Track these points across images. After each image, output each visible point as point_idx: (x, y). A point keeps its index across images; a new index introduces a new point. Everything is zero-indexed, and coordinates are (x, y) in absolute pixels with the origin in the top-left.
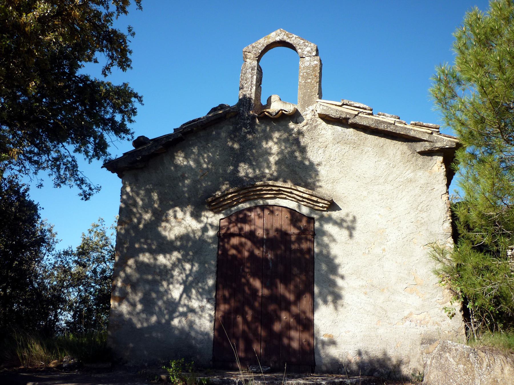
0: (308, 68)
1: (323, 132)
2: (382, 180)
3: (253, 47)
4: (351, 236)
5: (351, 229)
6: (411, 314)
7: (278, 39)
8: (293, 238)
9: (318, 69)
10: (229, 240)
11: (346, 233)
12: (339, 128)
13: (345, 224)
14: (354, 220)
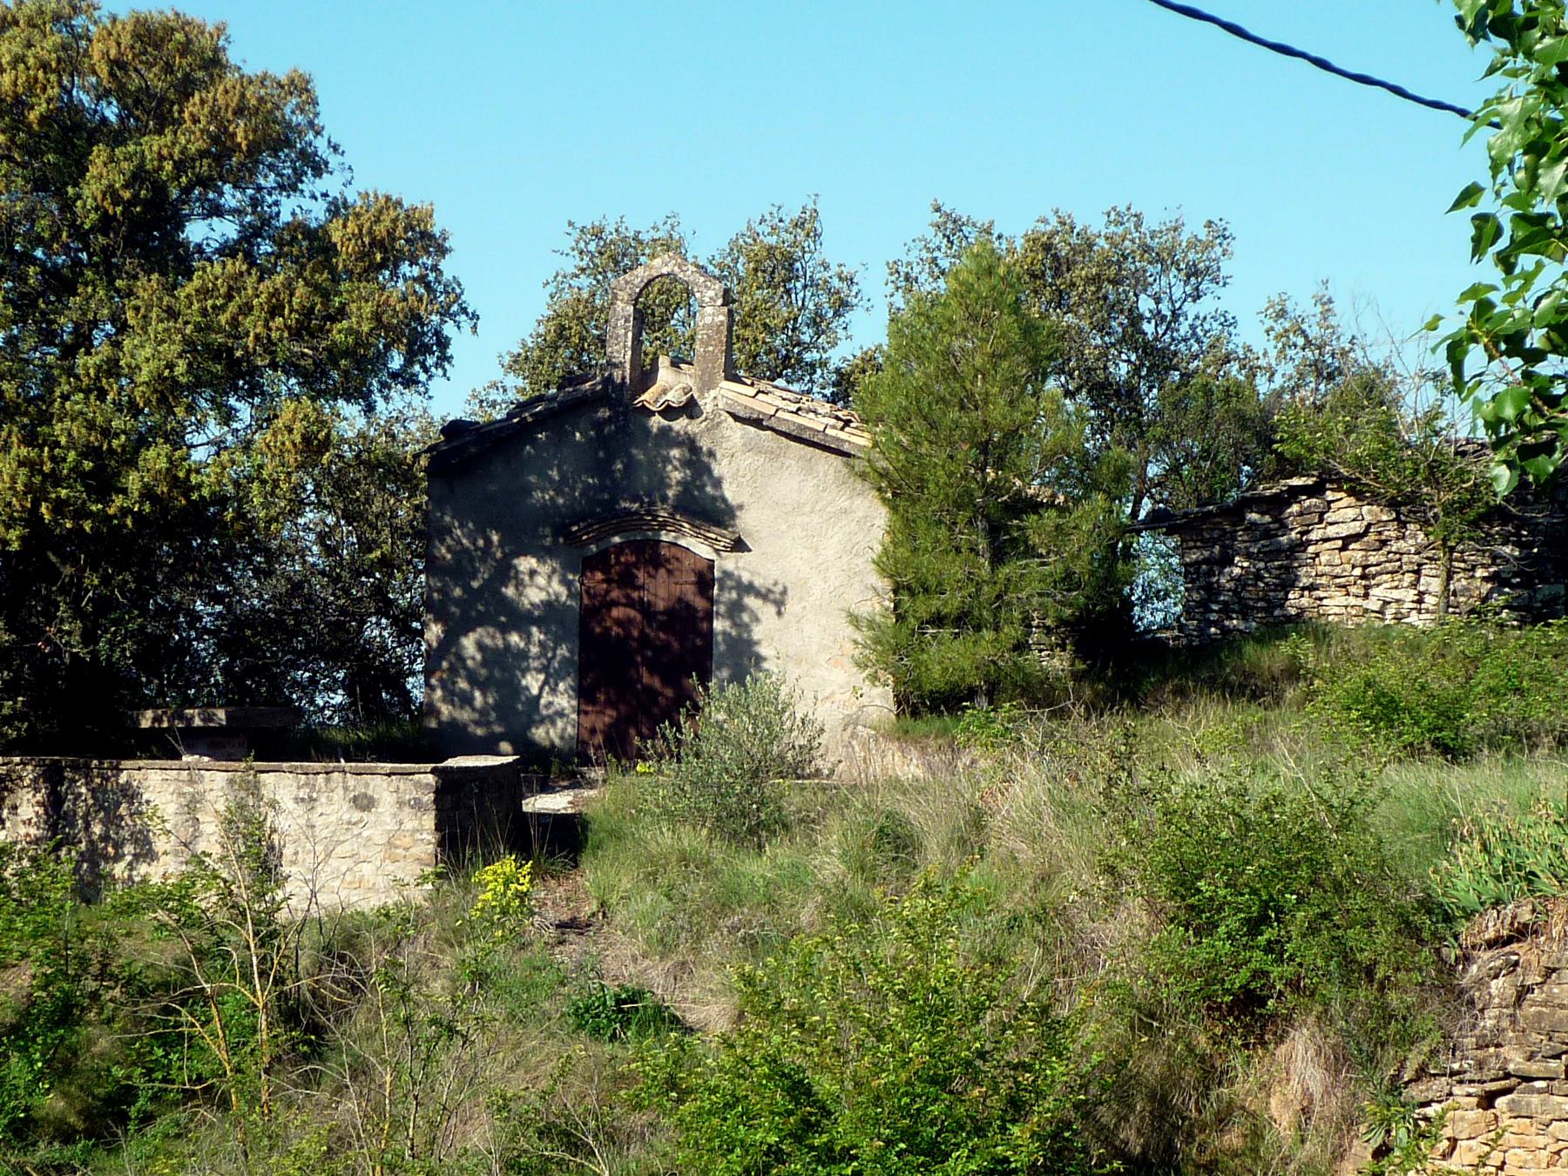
0: (709, 327)
1: (729, 433)
2: (807, 509)
3: (627, 283)
4: (779, 613)
5: (779, 604)
6: (833, 693)
7: (665, 271)
8: (700, 614)
9: (724, 329)
10: (609, 610)
11: (772, 609)
12: (752, 429)
13: (771, 596)
14: (784, 592)
